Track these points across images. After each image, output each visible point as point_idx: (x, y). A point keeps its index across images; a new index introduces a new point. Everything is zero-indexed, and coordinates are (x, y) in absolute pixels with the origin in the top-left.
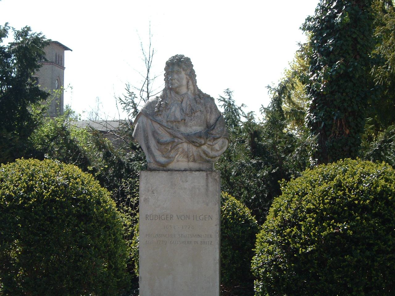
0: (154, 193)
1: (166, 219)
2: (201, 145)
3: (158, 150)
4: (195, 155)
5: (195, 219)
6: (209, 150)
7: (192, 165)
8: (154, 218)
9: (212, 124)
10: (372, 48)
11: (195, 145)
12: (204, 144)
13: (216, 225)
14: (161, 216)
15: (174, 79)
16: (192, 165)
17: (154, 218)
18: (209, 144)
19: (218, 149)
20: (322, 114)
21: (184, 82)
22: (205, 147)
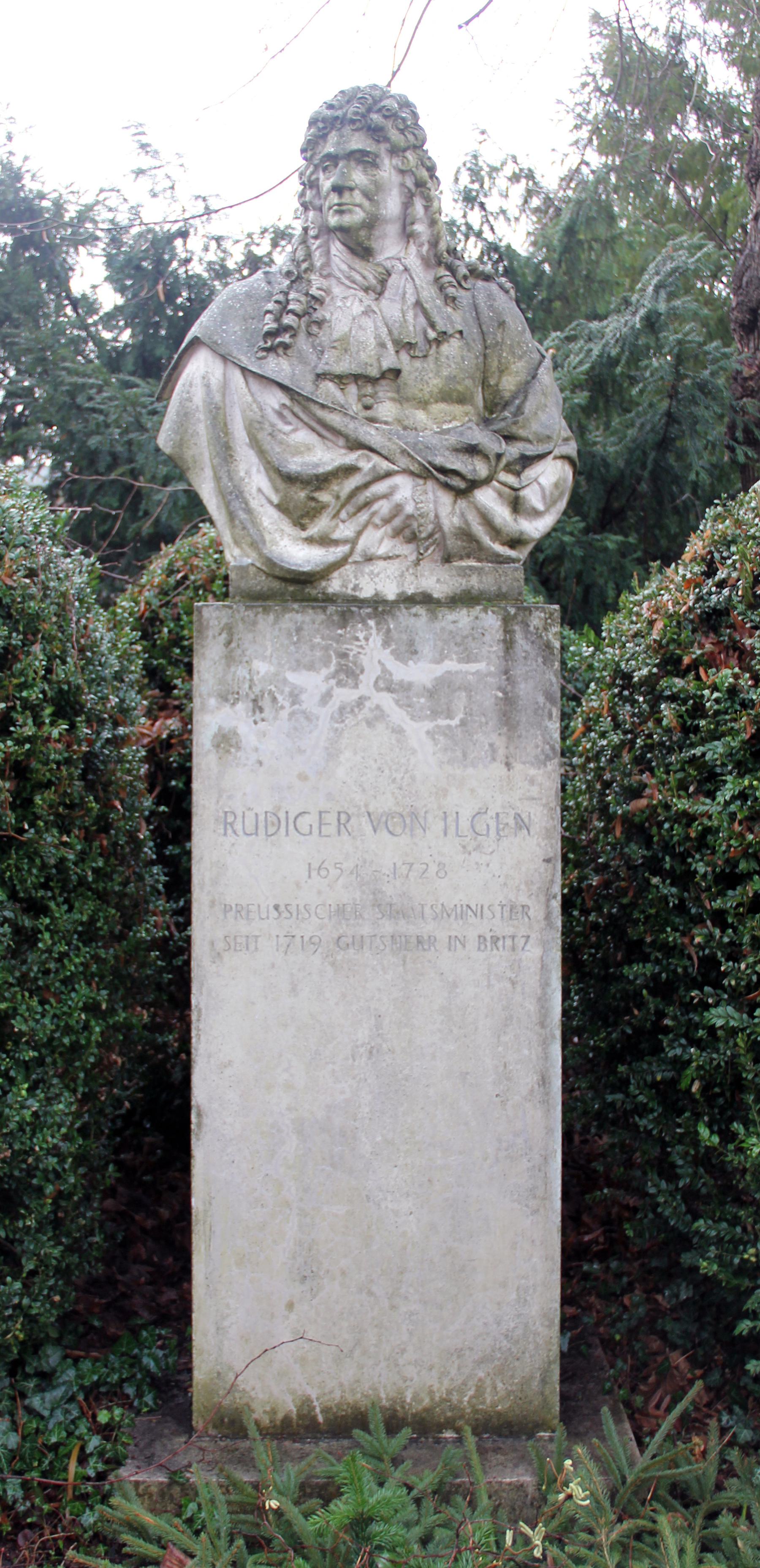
0: (261, 710)
1: (315, 830)
2: (474, 484)
3: (279, 507)
4: (446, 528)
5: (452, 830)
6: (502, 513)
7: (436, 580)
8: (261, 825)
9: (507, 395)
10: (315, 1416)
11: (447, 486)
12: (487, 481)
13: (548, 861)
14: (283, 830)
15: (351, 189)
16: (436, 580)
17: (261, 825)
18: (504, 484)
19: (540, 507)
20: (640, 1234)
21: (392, 205)
22: (486, 497)
